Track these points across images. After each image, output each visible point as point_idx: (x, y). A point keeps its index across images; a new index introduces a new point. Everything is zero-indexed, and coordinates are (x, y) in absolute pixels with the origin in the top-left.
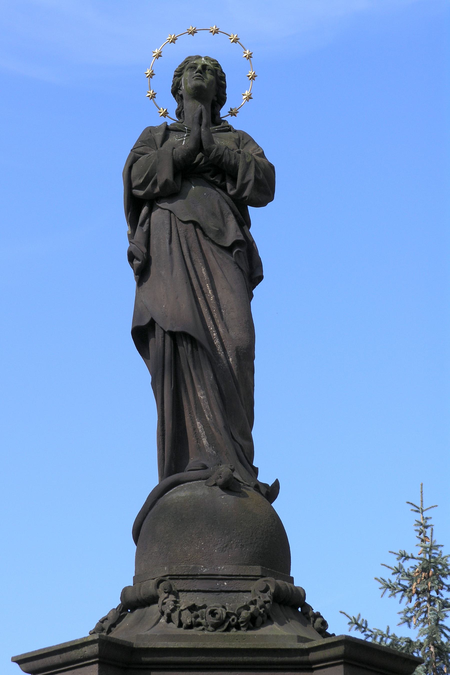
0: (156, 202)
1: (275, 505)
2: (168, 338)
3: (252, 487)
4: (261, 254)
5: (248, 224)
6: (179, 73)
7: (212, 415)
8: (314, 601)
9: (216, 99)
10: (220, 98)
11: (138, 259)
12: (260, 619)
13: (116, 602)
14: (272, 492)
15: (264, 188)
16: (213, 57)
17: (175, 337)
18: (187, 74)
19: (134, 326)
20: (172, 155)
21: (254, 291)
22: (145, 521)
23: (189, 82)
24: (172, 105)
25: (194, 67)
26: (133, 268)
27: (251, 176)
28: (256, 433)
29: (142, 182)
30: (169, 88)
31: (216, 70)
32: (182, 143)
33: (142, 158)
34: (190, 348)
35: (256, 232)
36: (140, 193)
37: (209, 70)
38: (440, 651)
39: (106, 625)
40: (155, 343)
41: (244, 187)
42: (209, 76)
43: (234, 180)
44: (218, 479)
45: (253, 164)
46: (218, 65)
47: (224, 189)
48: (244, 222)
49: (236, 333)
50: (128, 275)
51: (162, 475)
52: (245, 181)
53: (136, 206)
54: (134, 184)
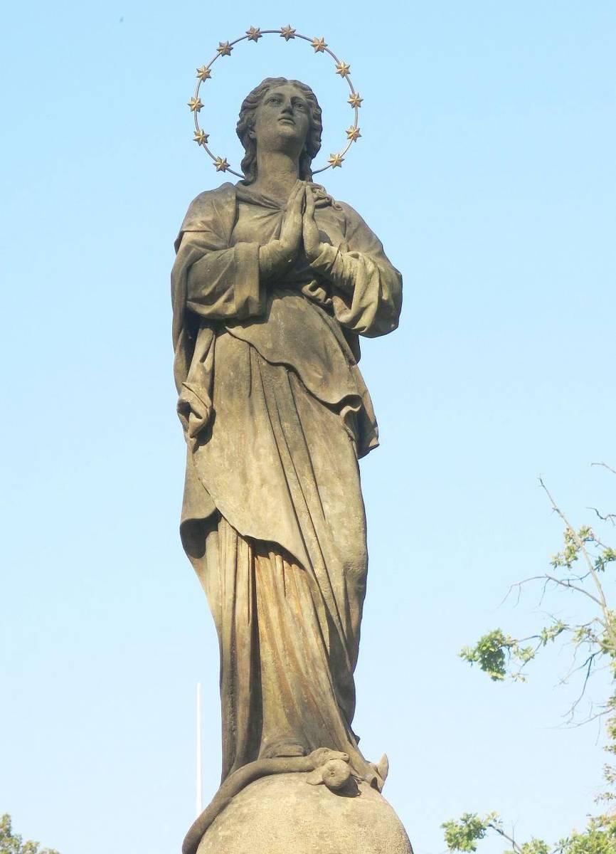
0: (225, 324)
2: (245, 550)
3: (367, 782)
5: (358, 357)
6: (250, 106)
7: (312, 670)
9: (306, 149)
11: (198, 416)
19: (184, 520)
20: (258, 259)
24: (236, 153)
25: (278, 100)
27: (373, 295)
29: (209, 295)
31: (310, 104)
34: (279, 566)
37: (300, 106)
40: (221, 547)
41: (361, 312)
42: (300, 116)
43: (348, 300)
44: (329, 776)
45: (376, 276)
46: (312, 96)
47: (330, 310)
49: (344, 540)
50: (176, 437)
52: (364, 305)
54: (190, 297)
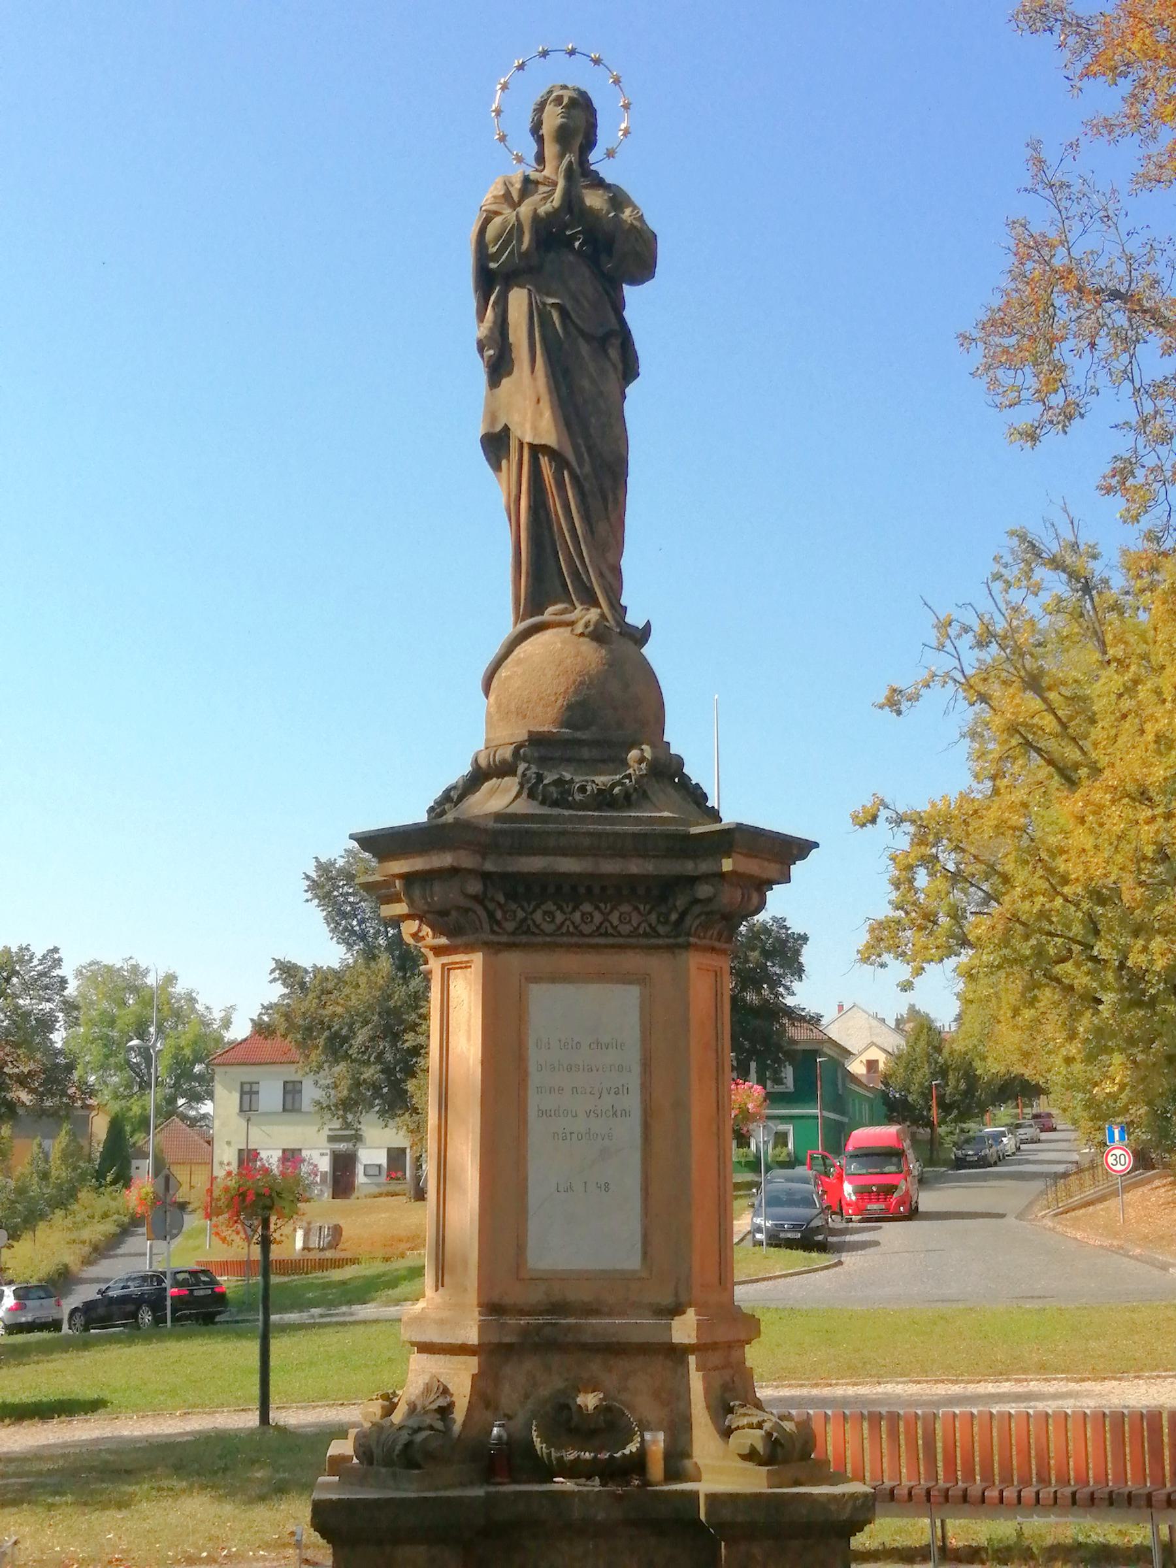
1: (646, 650)
4: (638, 346)
6: (540, 108)
8: (694, 771)
10: (590, 142)
12: (634, 796)
13: (466, 769)
14: (642, 635)
15: (642, 264)
16: (583, 88)
17: (536, 450)
18: (549, 108)
21: (627, 390)
22: (765, 1283)
23: (553, 118)
26: (482, 357)
28: (628, 563)
30: (528, 125)
32: (549, 202)
33: (498, 220)
35: (630, 315)
36: (493, 265)
38: (1102, 1187)
39: (454, 795)
48: (618, 305)
51: (518, 618)
53: (491, 280)
